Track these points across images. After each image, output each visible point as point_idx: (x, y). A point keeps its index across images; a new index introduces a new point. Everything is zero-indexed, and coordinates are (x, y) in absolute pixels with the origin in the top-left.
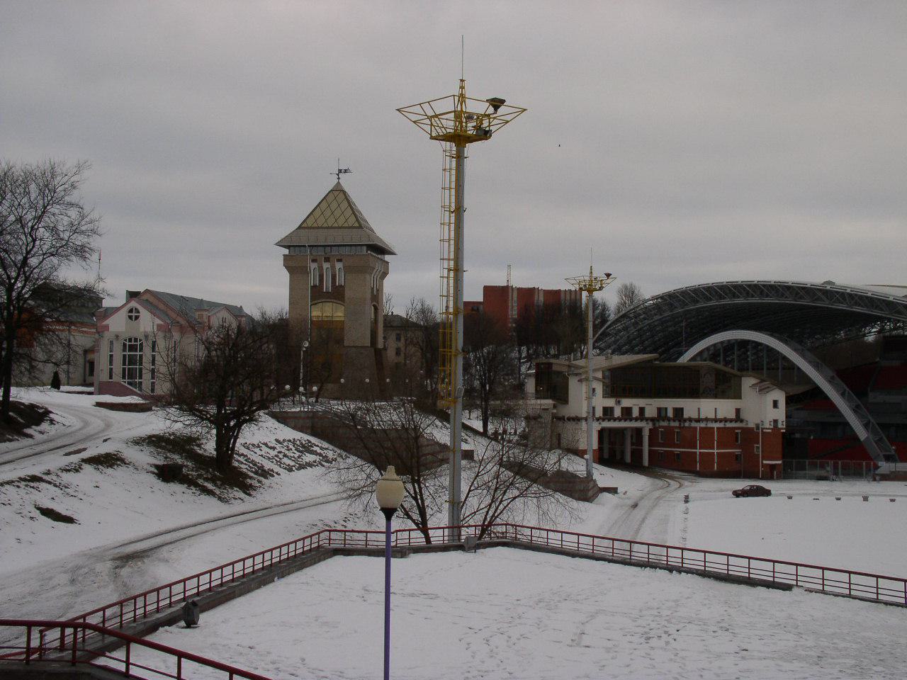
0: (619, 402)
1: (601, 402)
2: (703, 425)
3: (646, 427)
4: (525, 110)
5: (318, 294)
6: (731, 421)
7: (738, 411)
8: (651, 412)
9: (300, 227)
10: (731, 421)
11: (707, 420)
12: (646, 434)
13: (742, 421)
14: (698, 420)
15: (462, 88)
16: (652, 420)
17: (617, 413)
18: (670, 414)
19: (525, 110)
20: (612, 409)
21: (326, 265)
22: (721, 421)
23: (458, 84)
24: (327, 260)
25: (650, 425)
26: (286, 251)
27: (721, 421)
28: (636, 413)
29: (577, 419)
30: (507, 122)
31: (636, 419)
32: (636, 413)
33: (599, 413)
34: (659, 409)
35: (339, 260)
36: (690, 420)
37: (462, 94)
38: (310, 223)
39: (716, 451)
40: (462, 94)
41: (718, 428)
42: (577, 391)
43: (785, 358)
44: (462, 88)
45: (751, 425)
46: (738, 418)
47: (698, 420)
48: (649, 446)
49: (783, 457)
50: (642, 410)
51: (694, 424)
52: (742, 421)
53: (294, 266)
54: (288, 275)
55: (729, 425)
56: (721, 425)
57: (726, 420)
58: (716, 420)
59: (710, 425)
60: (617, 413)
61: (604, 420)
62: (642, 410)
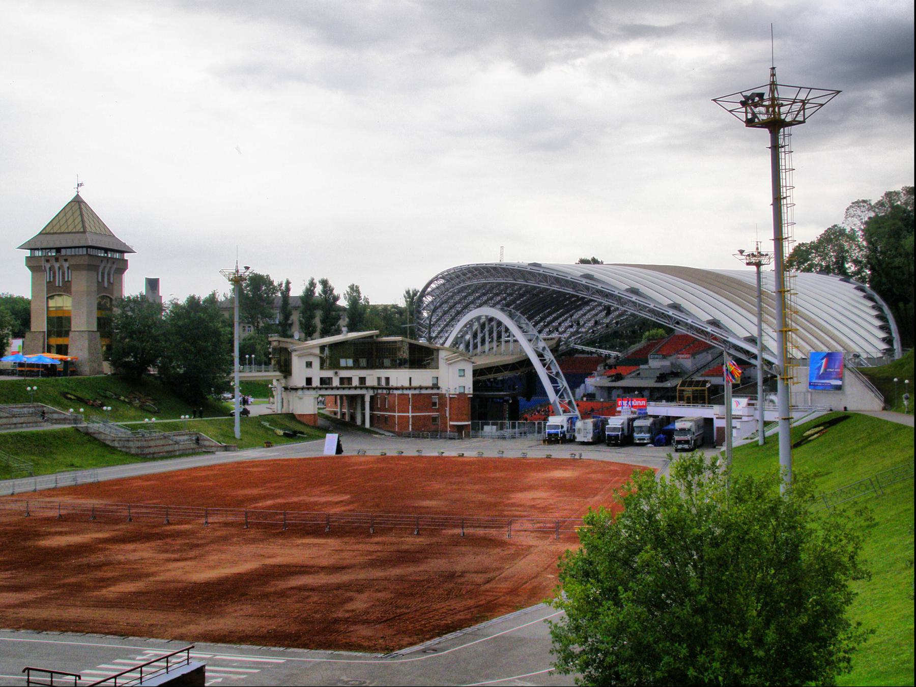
0: (336, 373)
1: (317, 374)
4: (714, 100)
6: (406, 389)
8: (371, 381)
9: (41, 234)
10: (406, 389)
11: (403, 388)
14: (397, 389)
15: (773, 75)
16: (373, 388)
17: (336, 382)
19: (714, 100)
20: (330, 379)
21: (57, 265)
22: (415, 388)
23: (769, 72)
25: (371, 393)
27: (415, 388)
28: (355, 382)
29: (296, 389)
30: (822, 105)
31: (356, 388)
32: (355, 382)
33: (316, 383)
35: (66, 260)
37: (773, 82)
38: (48, 230)
39: (410, 414)
40: (773, 82)
41: (413, 395)
42: (297, 365)
43: (333, 335)
44: (773, 75)
45: (444, 392)
46: (436, 386)
47: (397, 389)
48: (371, 409)
49: (472, 418)
50: (362, 380)
52: (438, 388)
53: (33, 264)
54: (30, 273)
56: (417, 392)
57: (421, 388)
58: (410, 389)
59: (405, 392)
60: (336, 382)
61: (320, 389)
62: (362, 380)
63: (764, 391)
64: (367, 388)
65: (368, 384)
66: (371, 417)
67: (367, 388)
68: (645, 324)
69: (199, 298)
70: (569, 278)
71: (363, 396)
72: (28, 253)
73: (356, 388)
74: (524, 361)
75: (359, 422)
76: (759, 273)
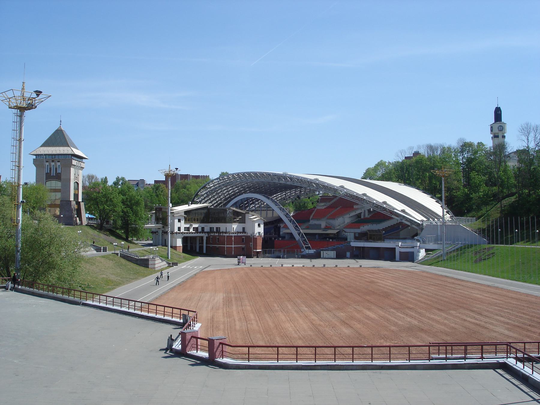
2: (228, 235)
3: (205, 236)
5: (49, 177)
6: (240, 233)
7: (244, 228)
8: (207, 229)
10: (240, 233)
12: (205, 239)
13: (245, 233)
14: (226, 233)
16: (208, 233)
18: (215, 230)
21: (53, 164)
24: (53, 161)
25: (207, 235)
26: (35, 157)
28: (200, 230)
31: (200, 232)
34: (211, 228)
36: (223, 232)
45: (249, 235)
50: (203, 228)
51: (224, 234)
55: (239, 234)
56: (236, 235)
57: (238, 233)
62: (203, 228)
63: (355, 233)
64: (205, 233)
65: (205, 230)
66: (207, 247)
67: (205, 233)
68: (406, 226)
69: (105, 181)
70: (326, 184)
71: (202, 237)
72: (35, 157)
73: (200, 232)
74: (279, 219)
75: (194, 249)
76: (482, 355)
